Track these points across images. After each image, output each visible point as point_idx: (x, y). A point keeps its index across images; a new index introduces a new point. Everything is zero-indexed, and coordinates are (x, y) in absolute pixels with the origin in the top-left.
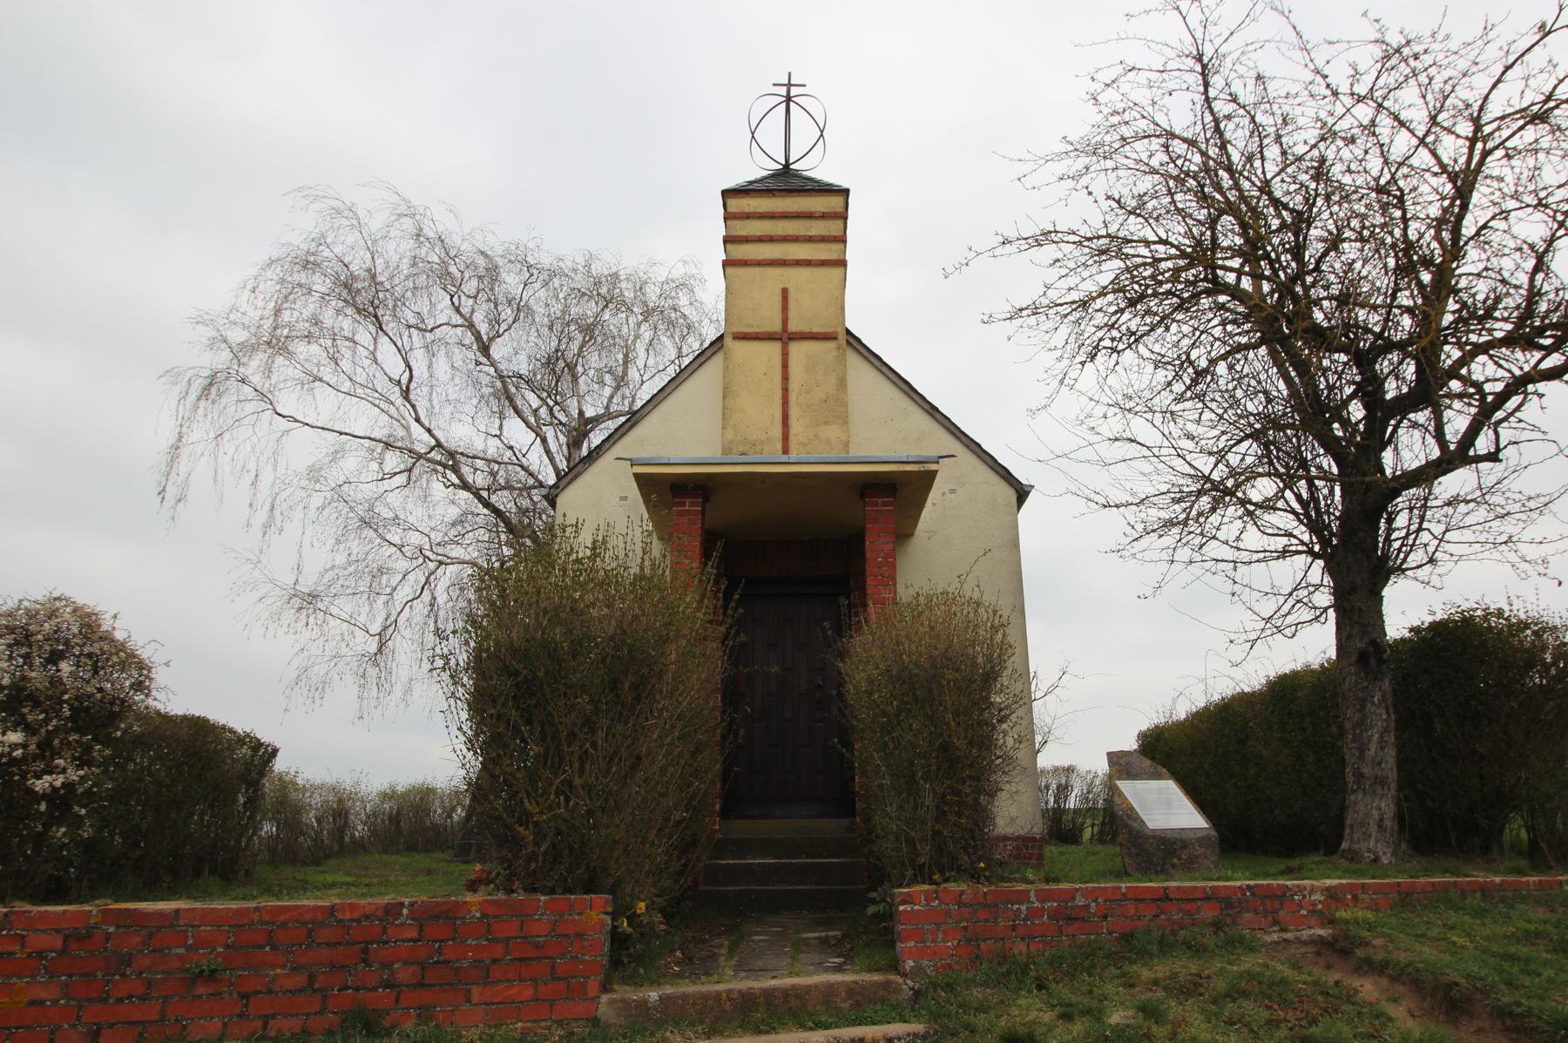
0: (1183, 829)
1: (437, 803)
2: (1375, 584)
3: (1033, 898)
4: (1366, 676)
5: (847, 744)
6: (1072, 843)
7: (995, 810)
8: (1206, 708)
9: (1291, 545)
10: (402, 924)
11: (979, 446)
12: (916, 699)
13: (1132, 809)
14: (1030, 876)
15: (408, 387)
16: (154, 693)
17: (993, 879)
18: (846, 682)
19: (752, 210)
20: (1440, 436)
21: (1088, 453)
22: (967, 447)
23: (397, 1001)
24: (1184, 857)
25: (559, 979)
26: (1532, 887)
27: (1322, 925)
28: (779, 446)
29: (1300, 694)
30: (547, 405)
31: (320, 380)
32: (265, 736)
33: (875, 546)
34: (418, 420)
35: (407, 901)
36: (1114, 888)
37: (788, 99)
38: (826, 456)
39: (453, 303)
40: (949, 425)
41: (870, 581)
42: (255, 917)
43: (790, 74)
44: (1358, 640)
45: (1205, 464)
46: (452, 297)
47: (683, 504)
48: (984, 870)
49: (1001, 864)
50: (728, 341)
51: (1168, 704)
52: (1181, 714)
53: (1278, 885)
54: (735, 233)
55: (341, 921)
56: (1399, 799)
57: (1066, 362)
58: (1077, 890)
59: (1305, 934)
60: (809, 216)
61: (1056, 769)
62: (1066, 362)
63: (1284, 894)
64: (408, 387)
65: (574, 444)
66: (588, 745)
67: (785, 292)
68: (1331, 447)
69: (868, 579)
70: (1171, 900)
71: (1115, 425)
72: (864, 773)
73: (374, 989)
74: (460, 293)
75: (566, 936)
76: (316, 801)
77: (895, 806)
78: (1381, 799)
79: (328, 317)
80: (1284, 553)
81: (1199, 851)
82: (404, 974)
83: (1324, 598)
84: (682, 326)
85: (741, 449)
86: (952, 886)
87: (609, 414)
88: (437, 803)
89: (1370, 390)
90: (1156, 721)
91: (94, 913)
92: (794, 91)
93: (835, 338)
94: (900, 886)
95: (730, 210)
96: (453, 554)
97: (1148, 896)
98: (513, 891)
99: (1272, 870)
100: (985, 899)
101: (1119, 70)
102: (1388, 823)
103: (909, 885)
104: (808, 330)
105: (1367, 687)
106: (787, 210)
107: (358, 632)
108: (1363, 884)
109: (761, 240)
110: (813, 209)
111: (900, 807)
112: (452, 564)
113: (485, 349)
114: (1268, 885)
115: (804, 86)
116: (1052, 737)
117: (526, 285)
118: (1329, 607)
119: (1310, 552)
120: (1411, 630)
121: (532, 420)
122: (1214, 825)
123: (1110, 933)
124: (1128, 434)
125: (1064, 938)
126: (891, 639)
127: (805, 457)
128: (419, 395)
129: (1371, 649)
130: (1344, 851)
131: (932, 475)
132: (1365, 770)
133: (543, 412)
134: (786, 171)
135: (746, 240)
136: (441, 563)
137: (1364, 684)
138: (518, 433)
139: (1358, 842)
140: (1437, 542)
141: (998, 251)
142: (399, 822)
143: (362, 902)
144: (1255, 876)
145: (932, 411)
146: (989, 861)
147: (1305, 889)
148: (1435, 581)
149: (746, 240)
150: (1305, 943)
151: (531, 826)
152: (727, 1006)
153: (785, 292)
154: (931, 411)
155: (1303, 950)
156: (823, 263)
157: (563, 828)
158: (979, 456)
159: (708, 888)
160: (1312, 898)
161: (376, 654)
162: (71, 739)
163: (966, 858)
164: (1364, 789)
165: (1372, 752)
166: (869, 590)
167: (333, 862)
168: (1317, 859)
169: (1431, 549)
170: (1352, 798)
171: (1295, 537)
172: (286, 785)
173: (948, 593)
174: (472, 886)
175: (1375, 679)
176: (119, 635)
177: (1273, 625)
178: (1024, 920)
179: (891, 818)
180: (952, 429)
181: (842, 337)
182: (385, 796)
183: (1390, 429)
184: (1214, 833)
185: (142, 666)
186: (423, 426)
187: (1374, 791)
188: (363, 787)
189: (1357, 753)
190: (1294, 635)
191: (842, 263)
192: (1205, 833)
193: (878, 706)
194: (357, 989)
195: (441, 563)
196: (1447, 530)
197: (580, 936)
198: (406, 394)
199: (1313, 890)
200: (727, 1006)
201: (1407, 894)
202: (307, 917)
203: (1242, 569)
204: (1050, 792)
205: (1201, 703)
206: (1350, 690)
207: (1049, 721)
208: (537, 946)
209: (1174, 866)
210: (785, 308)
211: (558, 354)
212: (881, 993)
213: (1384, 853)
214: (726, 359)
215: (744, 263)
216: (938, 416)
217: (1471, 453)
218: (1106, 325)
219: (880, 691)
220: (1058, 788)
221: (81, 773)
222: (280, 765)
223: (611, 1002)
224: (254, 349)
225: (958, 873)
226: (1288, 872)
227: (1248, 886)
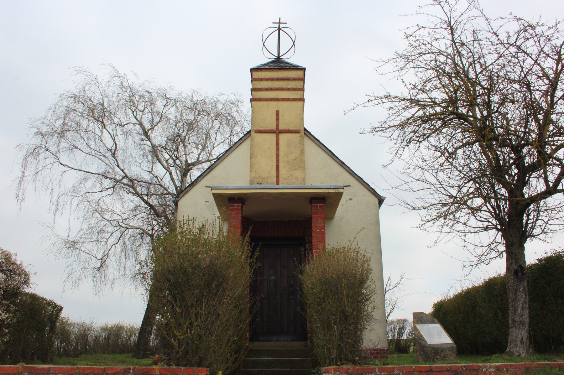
0: (442, 344)
1: (124, 334)
2: (521, 242)
3: (377, 371)
4: (517, 280)
5: (303, 309)
6: (405, 353)
7: (363, 337)
8: (461, 293)
9: (489, 225)
11: (362, 179)
12: (331, 292)
13: (422, 336)
14: (377, 363)
15: (114, 152)
16: (31, 285)
17: (361, 364)
18: (303, 284)
19: (263, 77)
20: (546, 181)
21: (405, 187)
22: (357, 180)
28: (275, 179)
29: (496, 287)
30: (173, 159)
31: (77, 148)
32: (58, 302)
33: (316, 225)
34: (118, 166)
35: (132, 367)
36: (410, 367)
37: (279, 29)
38: (295, 185)
39: (134, 115)
40: (348, 169)
41: (314, 240)
42: (77, 371)
43: (280, 18)
44: (514, 265)
45: (454, 192)
46: (133, 112)
47: (233, 206)
48: (358, 360)
49: (365, 358)
50: (253, 134)
51: (446, 291)
52: (451, 295)
54: (256, 87)
55: (108, 374)
56: (529, 330)
57: (398, 145)
58: (395, 368)
60: (288, 79)
61: (398, 321)
62: (398, 145)
63: (479, 369)
64: (114, 152)
65: (184, 175)
66: (199, 309)
67: (277, 112)
68: (506, 185)
69: (313, 239)
70: (433, 371)
71: (418, 173)
72: (310, 322)
74: (137, 110)
76: (75, 330)
77: (322, 335)
79: (84, 123)
80: (487, 229)
81: (448, 353)
83: (502, 248)
84: (231, 122)
85: (258, 181)
86: (345, 366)
87: (199, 161)
88: (124, 334)
89: (519, 161)
90: (441, 299)
91: (20, 368)
92: (282, 26)
93: (299, 132)
94: (324, 367)
95: (254, 77)
96: (131, 224)
97: (424, 370)
98: (170, 365)
99: (479, 360)
101: (417, 28)
102: (525, 340)
103: (327, 366)
104: (287, 129)
105: (518, 285)
106: (279, 77)
107: (93, 258)
108: (511, 365)
109: (267, 90)
110: (290, 77)
111: (324, 335)
112: (132, 228)
113: (146, 133)
115: (286, 23)
116: (397, 306)
117: (165, 106)
118: (504, 251)
119: (496, 228)
120: (538, 260)
121: (165, 164)
122: (456, 343)
124: (423, 178)
126: (321, 267)
127: (286, 186)
128: (119, 153)
129: (519, 269)
130: (507, 352)
131: (341, 194)
132: (516, 319)
133: (171, 161)
134: (278, 59)
135: (261, 90)
136: (127, 228)
138: (159, 170)
139: (513, 348)
140: (545, 224)
141: (366, 105)
142: (109, 340)
143: (115, 367)
145: (342, 164)
146: (360, 357)
148: (548, 240)
149: (261, 90)
151: (177, 341)
153: (277, 112)
154: (341, 164)
156: (294, 100)
157: (189, 341)
158: (362, 184)
159: (244, 369)
161: (100, 268)
162: (4, 302)
163: (350, 355)
164: (516, 327)
165: (519, 311)
166: (313, 244)
167: (83, 356)
168: (496, 355)
169: (543, 228)
170: (511, 330)
171: (490, 222)
172: (65, 323)
173: (345, 248)
174: (155, 363)
175: (521, 281)
176: (18, 263)
177: (482, 259)
179: (320, 340)
180: (351, 172)
181: (302, 131)
182: (104, 329)
183: (527, 178)
184: (455, 345)
185: (26, 275)
186: (120, 169)
187: (519, 327)
188: (94, 325)
189: (513, 312)
190: (489, 263)
191: (303, 100)
192: (451, 345)
193: (316, 294)
195: (127, 228)
196: (548, 220)
198: (114, 155)
199: (490, 367)
201: (529, 368)
202: (96, 372)
203: (468, 235)
204: (396, 330)
205: (459, 290)
206: (511, 286)
207: (395, 300)
209: (438, 359)
210: (277, 119)
211: (179, 136)
213: (523, 353)
214: (252, 141)
218: (414, 131)
219: (316, 288)
220: (399, 329)
221: (7, 316)
222: (63, 314)
224: (52, 134)
225: (347, 361)
226: (484, 361)
227: (464, 366)
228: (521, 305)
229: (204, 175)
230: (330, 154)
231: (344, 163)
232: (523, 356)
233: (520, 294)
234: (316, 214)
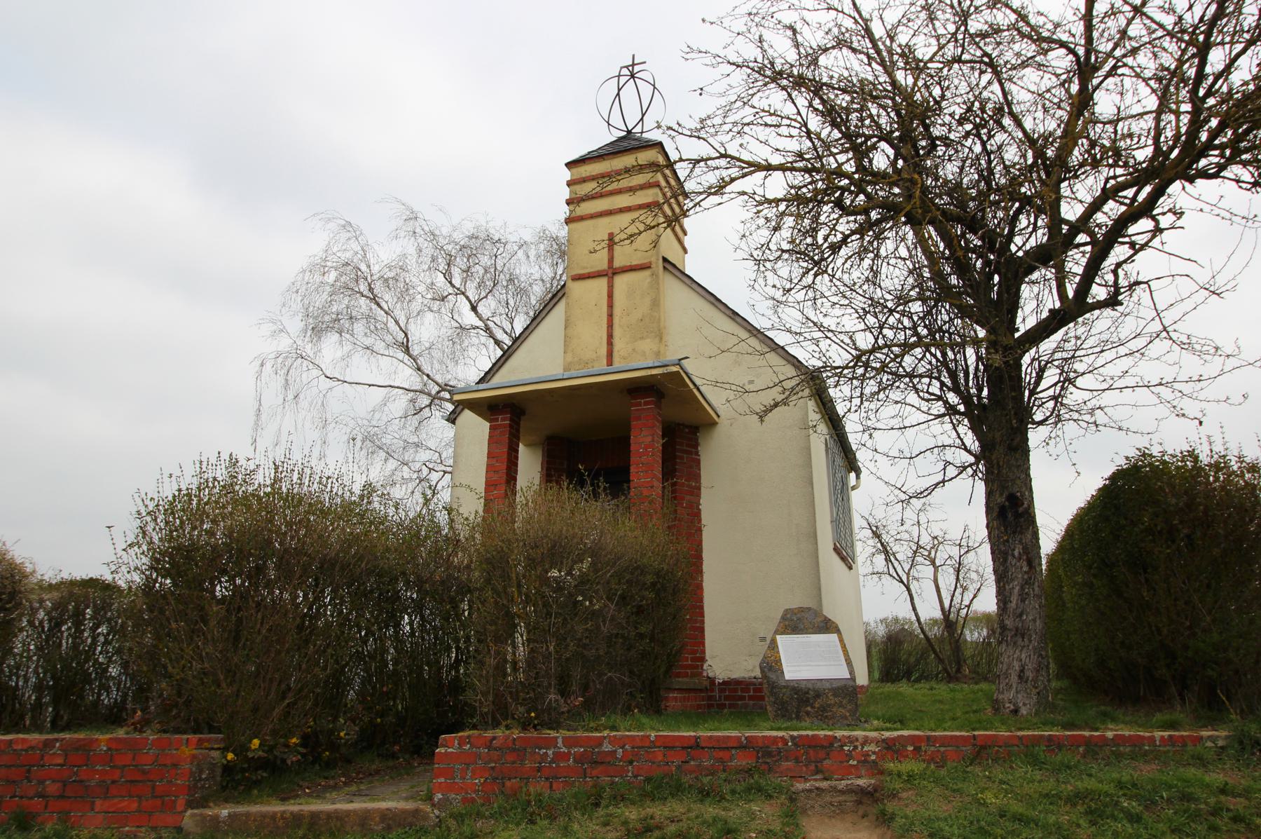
4: (1006, 529)
10: (54, 754)
23: (46, 807)
24: (817, 705)
25: (156, 797)
26: (1158, 743)
27: (872, 775)
28: (605, 362)
50: (570, 284)
53: (825, 736)
59: (842, 784)
63: (831, 745)
73: (32, 798)
75: (165, 765)
78: (1021, 651)
82: (52, 788)
100: (514, 744)
102: (1030, 674)
105: (1007, 541)
114: (813, 736)
123: (636, 776)
125: (588, 779)
137: (1005, 538)
139: (1003, 693)
144: (670, 729)
145: (734, 315)
147: (857, 740)
150: (842, 792)
152: (281, 823)
155: (841, 798)
160: (865, 749)
165: (1013, 605)
175: (1014, 533)
178: (550, 763)
187: (1015, 643)
194: (21, 797)
197: (175, 765)
199: (866, 741)
200: (281, 823)
208: (144, 772)
209: (808, 713)
212: (410, 820)
213: (1024, 704)
215: (581, 218)
216: (739, 320)
217: (1090, 300)
223: (193, 815)
228: (1017, 588)
229: (495, 369)
230: (712, 299)
231: (738, 314)
232: (1025, 713)
233: (1013, 563)
234: (638, 418)
